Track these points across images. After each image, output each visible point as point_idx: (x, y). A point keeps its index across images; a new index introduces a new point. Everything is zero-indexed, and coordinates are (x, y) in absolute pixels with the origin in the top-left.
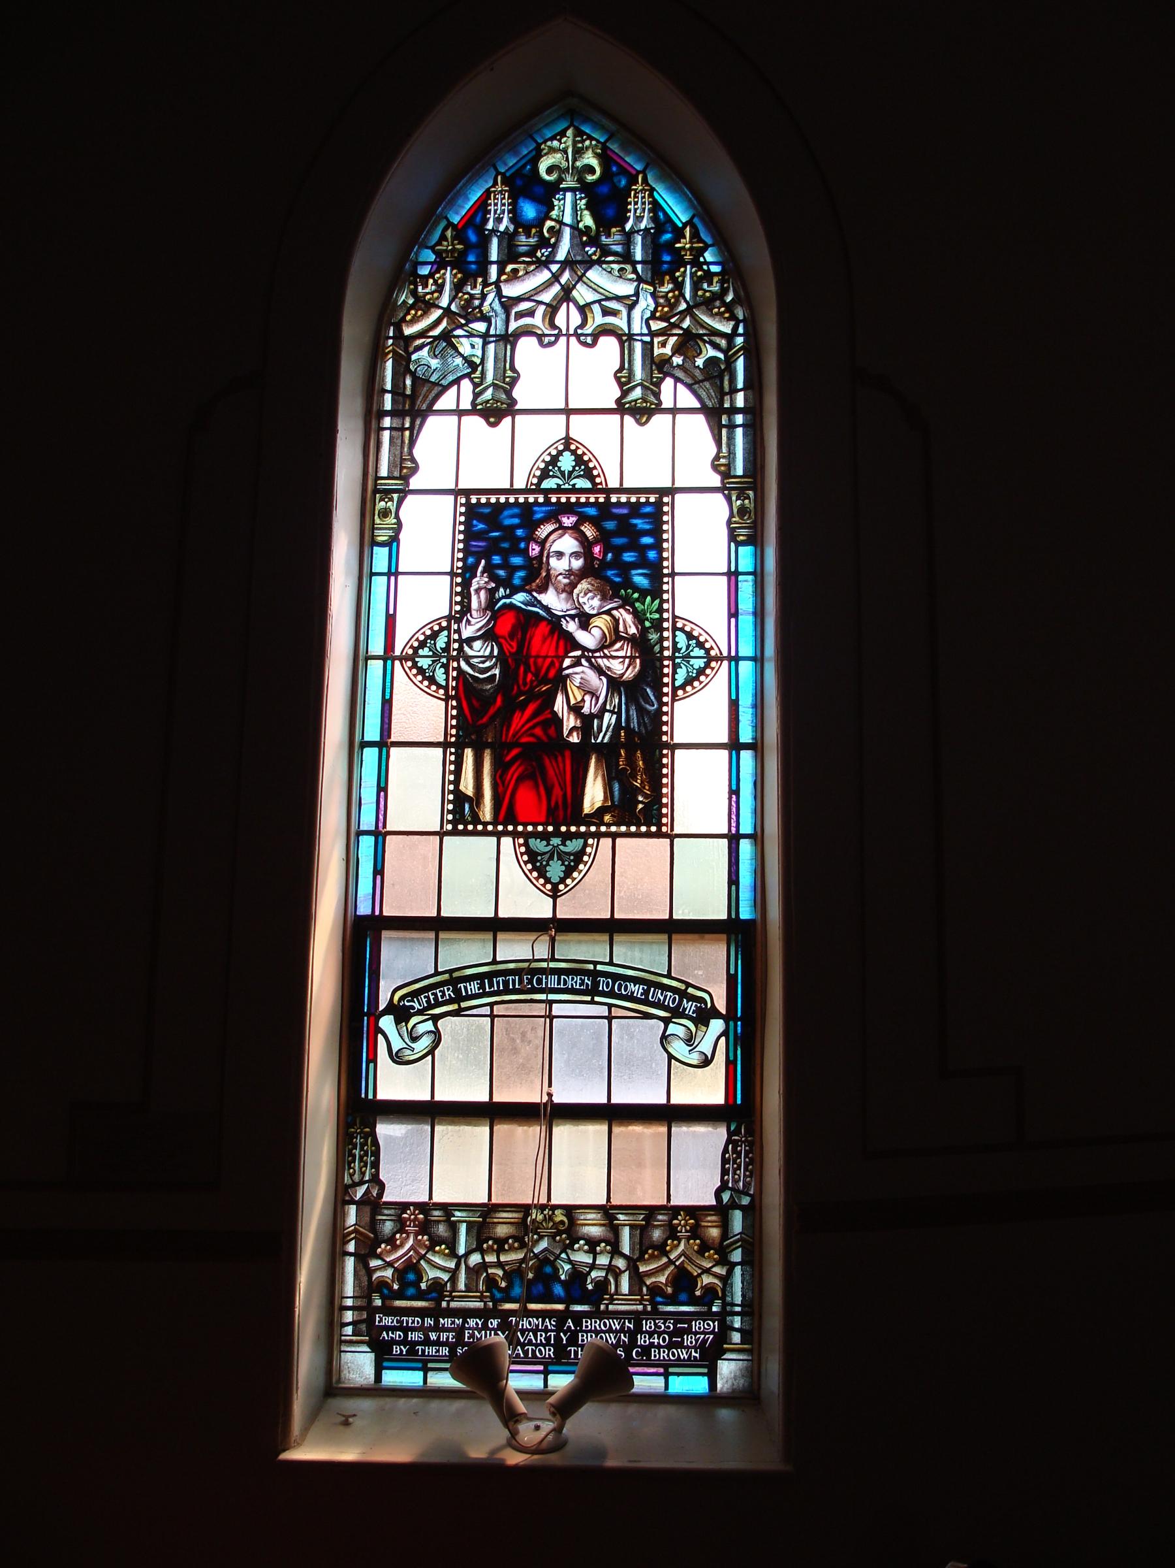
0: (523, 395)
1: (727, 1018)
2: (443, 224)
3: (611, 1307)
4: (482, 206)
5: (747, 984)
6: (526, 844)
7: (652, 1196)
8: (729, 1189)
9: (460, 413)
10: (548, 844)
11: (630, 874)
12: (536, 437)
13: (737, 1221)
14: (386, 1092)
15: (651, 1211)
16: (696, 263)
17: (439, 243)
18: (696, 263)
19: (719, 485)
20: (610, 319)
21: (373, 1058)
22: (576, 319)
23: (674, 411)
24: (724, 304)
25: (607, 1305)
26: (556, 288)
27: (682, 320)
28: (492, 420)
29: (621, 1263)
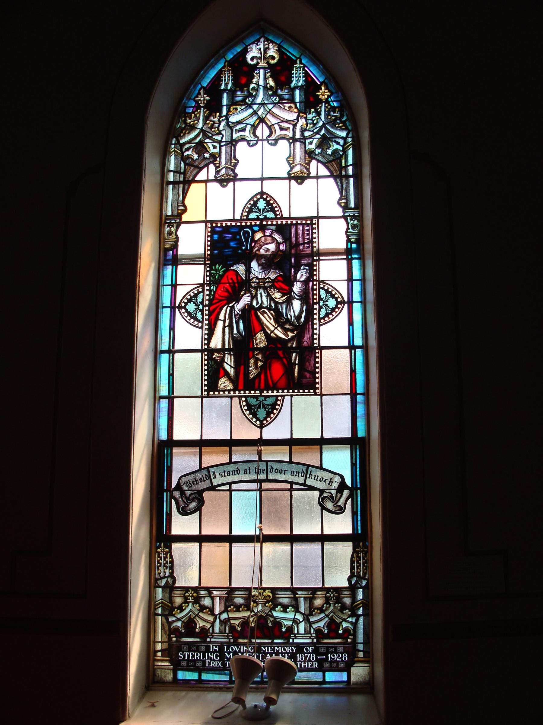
0: (240, 171)
3: (295, 641)
9: (206, 182)
11: (300, 416)
12: (245, 192)
13: (360, 595)
22: (267, 132)
23: (317, 177)
24: (342, 122)
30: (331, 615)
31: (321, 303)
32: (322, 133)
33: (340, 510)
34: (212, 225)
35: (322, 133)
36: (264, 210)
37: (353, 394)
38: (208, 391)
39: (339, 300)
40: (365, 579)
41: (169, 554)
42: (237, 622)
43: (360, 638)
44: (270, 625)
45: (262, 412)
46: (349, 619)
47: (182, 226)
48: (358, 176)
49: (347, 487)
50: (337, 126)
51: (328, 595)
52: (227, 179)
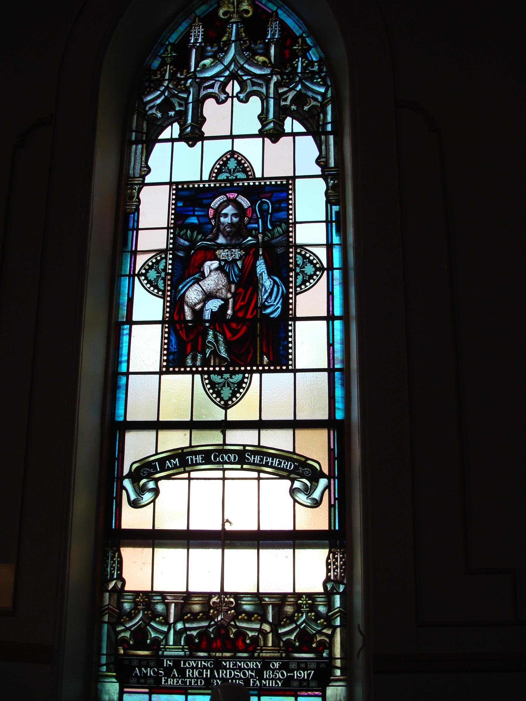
0: (207, 130)
1: (329, 478)
3: (261, 654)
4: (187, 35)
5: (339, 455)
6: (209, 378)
7: (285, 587)
8: (332, 581)
9: (172, 140)
10: (222, 378)
11: (269, 393)
12: (215, 150)
13: (337, 601)
14: (126, 524)
15: (283, 596)
16: (305, 57)
17: (164, 53)
18: (305, 57)
19: (320, 173)
20: (255, 88)
22: (237, 88)
23: (294, 135)
24: (320, 77)
25: (259, 653)
27: (296, 86)
28: (190, 143)
29: (267, 627)
30: (303, 626)
31: (298, 270)
32: (298, 89)
34: (177, 187)
35: (298, 89)
36: (234, 170)
37: (331, 371)
39: (318, 266)
40: (343, 584)
41: (117, 554)
42: (194, 633)
43: (338, 653)
44: (232, 636)
45: (226, 394)
46: (325, 631)
47: (145, 188)
48: (337, 132)
50: (315, 81)
51: (300, 602)
52: (194, 136)
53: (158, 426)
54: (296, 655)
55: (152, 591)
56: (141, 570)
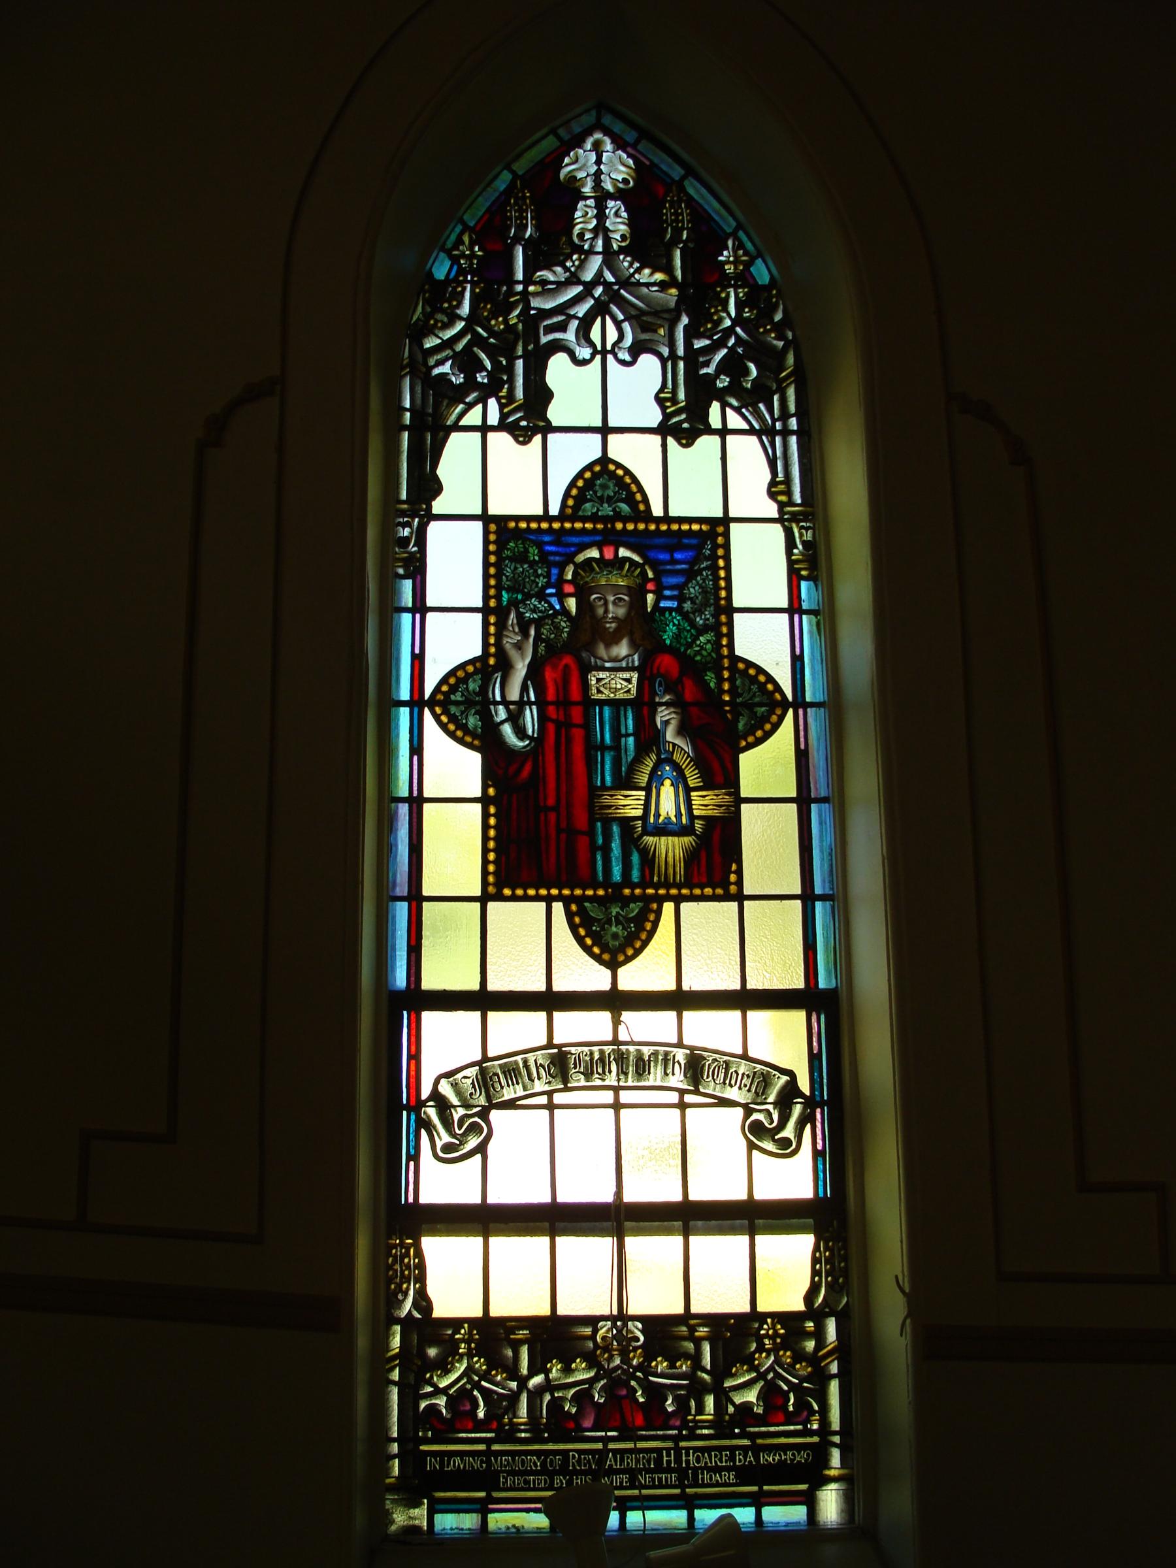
0: (556, 414)
2: (459, 228)
11: (698, 943)
12: (572, 456)
19: (776, 516)
21: (415, 1157)
26: (589, 303)
33: (787, 1149)
38: (499, 885)
49: (801, 1094)
52: (531, 419)
53: (483, 1000)
54: (752, 1429)
55: (755, 1316)
56: (453, 1278)
